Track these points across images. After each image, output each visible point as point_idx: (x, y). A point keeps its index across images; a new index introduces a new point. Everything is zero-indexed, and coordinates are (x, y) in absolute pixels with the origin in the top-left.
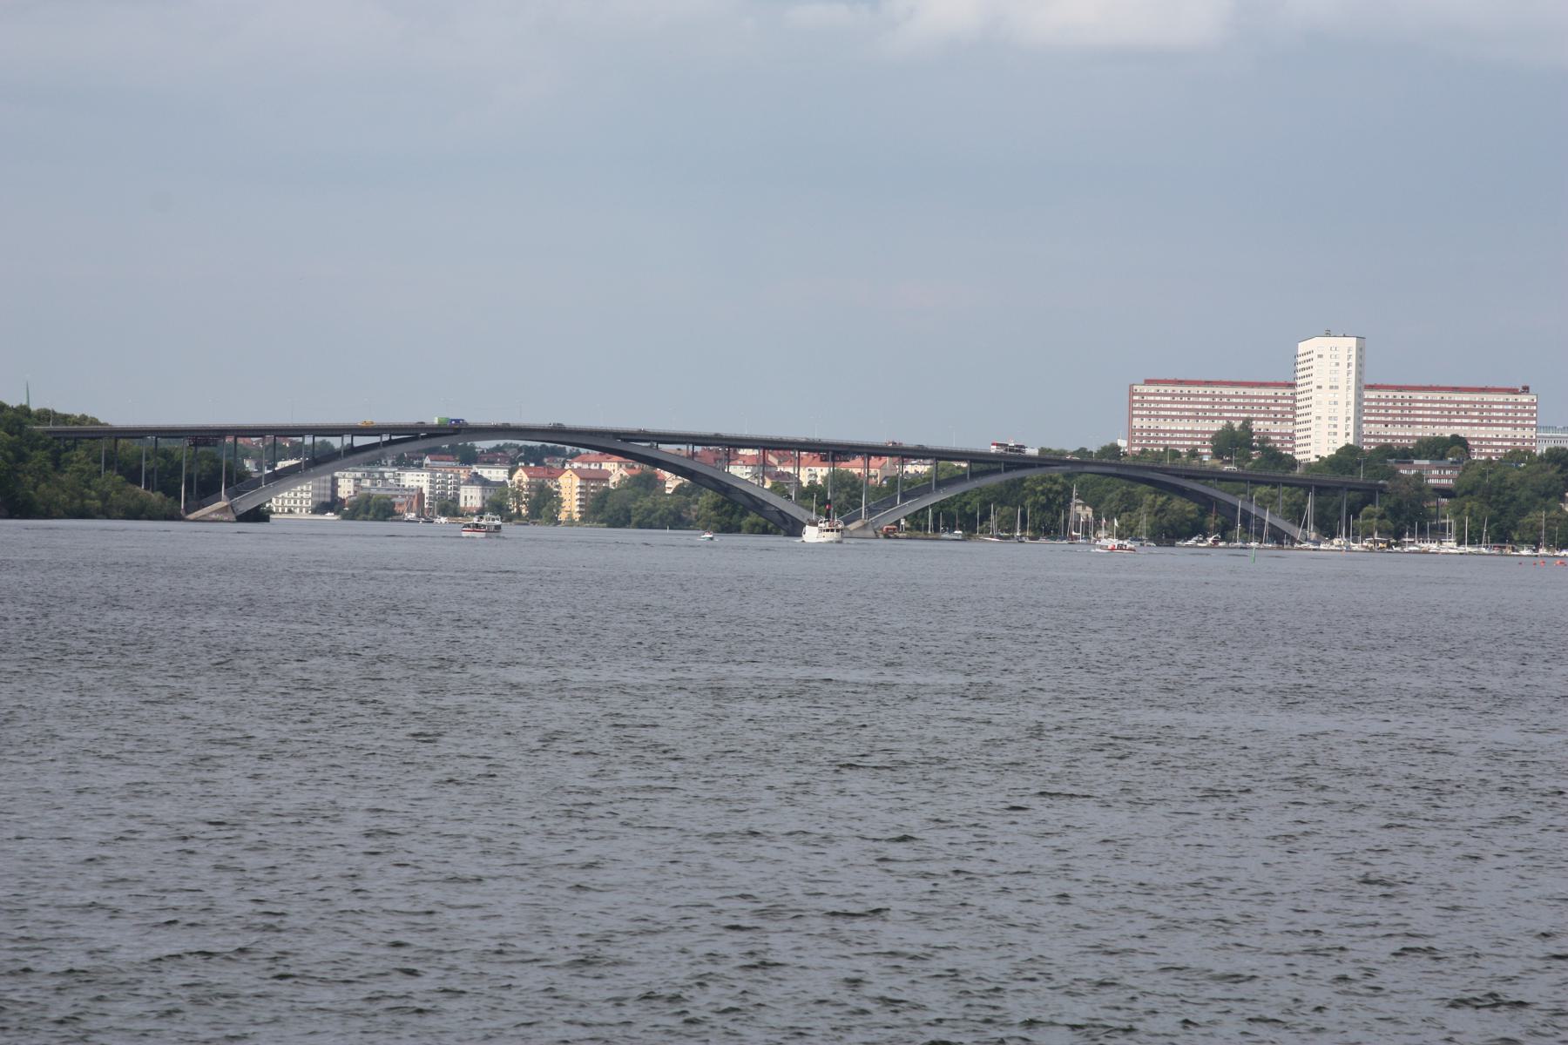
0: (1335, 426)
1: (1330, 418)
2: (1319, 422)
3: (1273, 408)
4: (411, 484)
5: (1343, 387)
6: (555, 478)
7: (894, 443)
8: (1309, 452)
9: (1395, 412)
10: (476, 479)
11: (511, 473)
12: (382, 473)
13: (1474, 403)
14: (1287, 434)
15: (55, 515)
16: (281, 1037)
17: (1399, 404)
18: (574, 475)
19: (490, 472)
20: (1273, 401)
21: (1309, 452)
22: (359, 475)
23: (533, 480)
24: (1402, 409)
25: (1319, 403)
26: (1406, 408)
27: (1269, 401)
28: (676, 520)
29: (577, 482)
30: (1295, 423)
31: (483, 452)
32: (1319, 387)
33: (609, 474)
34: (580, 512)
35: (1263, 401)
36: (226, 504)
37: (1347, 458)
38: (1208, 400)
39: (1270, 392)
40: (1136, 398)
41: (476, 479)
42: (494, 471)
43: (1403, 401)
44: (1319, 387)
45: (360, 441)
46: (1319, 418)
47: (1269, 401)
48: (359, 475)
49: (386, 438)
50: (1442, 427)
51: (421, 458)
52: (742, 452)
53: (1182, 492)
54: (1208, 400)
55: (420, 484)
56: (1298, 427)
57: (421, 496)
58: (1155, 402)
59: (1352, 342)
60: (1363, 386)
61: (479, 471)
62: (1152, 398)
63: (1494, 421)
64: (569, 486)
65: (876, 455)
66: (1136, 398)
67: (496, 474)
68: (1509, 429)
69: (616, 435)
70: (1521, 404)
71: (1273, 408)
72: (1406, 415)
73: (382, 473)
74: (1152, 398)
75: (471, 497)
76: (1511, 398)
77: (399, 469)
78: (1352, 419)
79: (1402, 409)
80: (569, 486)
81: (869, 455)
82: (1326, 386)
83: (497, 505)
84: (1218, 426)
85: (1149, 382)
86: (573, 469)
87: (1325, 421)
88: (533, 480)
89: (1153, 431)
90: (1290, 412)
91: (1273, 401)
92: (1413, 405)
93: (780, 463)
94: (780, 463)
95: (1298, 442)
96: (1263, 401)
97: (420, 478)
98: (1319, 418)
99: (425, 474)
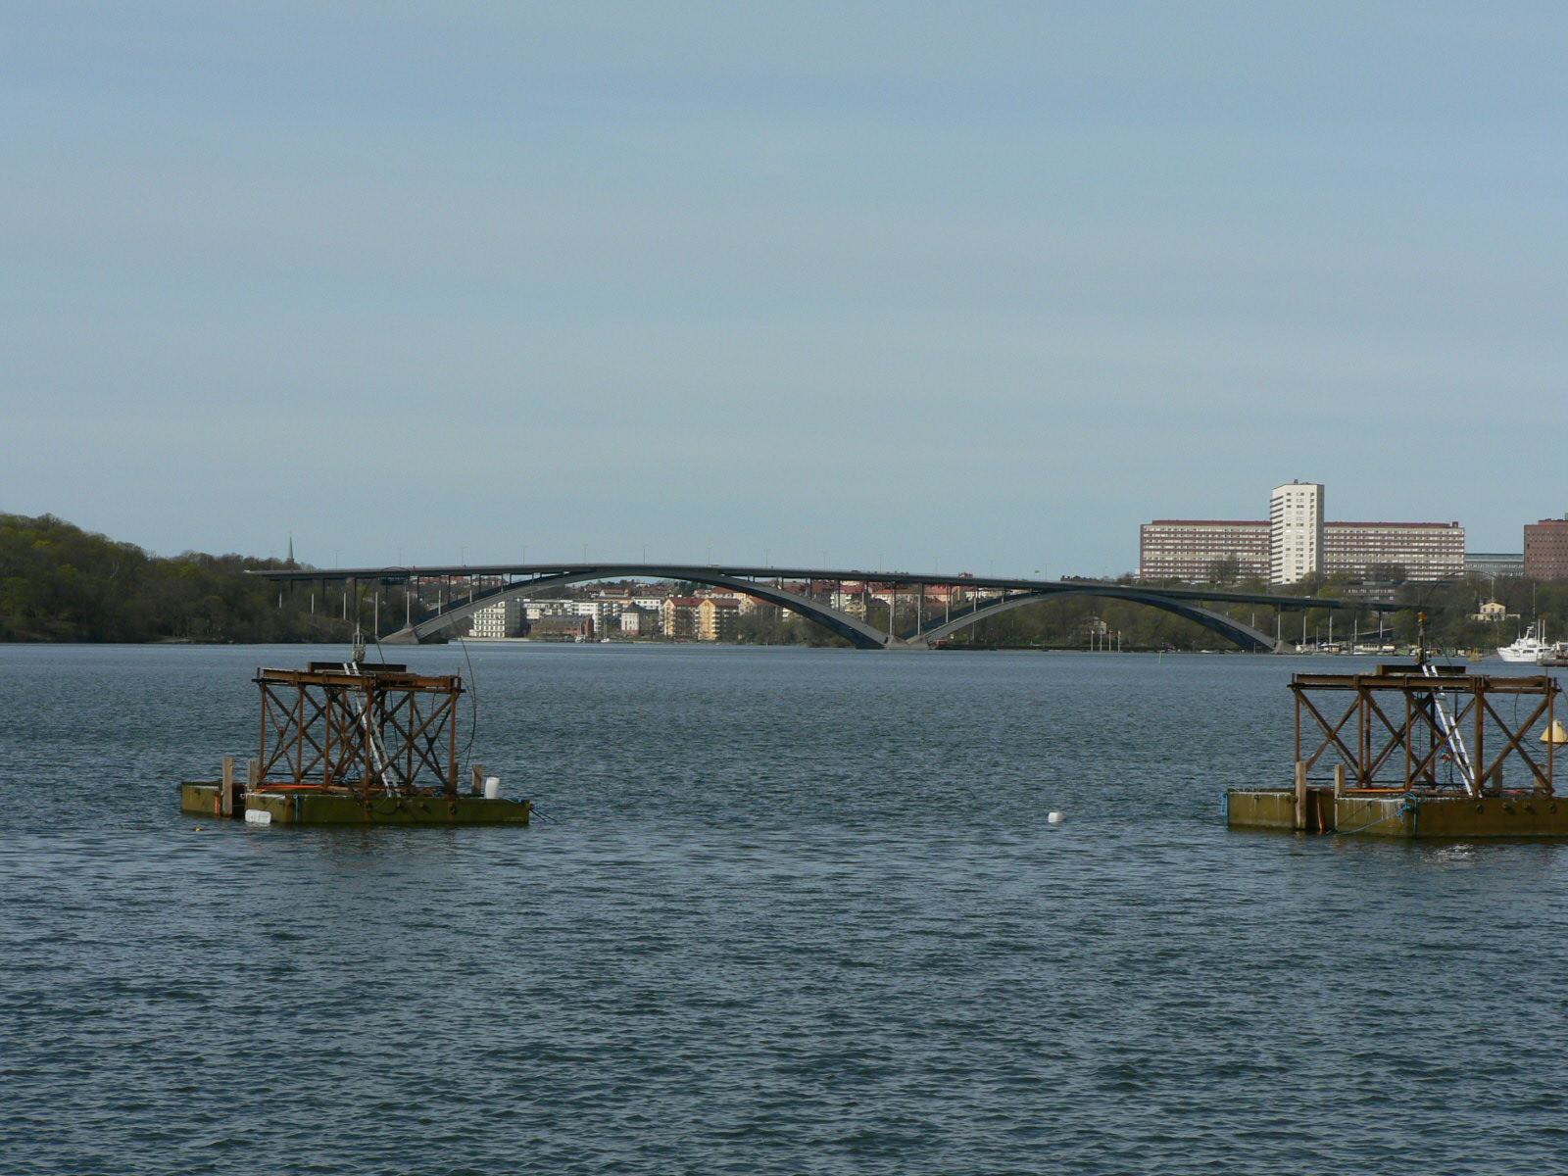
0: (1302, 556)
1: (1297, 549)
2: (1288, 552)
3: (1255, 542)
4: (583, 612)
5: (1307, 524)
6: (696, 607)
7: (966, 575)
8: (1280, 577)
9: (1221, 542)
10: (634, 608)
11: (663, 602)
12: (562, 604)
13: (1257, 534)
14: (1266, 563)
15: (326, 641)
16: (64, 1132)
17: (1355, 538)
18: (711, 604)
19: (645, 602)
20: (1255, 537)
21: (1280, 577)
22: (543, 606)
23: (679, 608)
24: (1358, 541)
25: (1288, 537)
26: (1361, 541)
27: (1251, 537)
28: (790, 638)
29: (713, 609)
30: (1271, 554)
31: (646, 586)
32: (1289, 525)
33: (739, 602)
34: (716, 633)
35: (1246, 536)
36: (410, 630)
37: (1313, 582)
38: (1436, 539)
39: (1252, 529)
40: (1146, 535)
41: (634, 608)
42: (649, 601)
43: (1358, 535)
44: (1289, 525)
45: (516, 578)
46: (1288, 549)
47: (1251, 537)
48: (543, 606)
49: (537, 576)
50: (1390, 556)
51: (598, 592)
52: (845, 583)
53: (1174, 609)
54: (1436, 539)
55: (590, 613)
56: (1274, 557)
57: (591, 622)
58: (1161, 538)
59: (1314, 489)
60: (1322, 524)
61: (637, 601)
62: (1158, 535)
63: (1217, 548)
64: (707, 615)
65: (929, 584)
66: (1146, 535)
67: (650, 603)
68: (1158, 553)
69: (720, 571)
70: (1452, 536)
71: (1255, 542)
72: (1361, 547)
73: (562, 604)
74: (1158, 535)
75: (630, 622)
76: (1444, 532)
77: (574, 601)
78: (1315, 550)
79: (1358, 541)
80: (707, 615)
81: (924, 583)
82: (1294, 524)
83: (650, 628)
84: (1211, 556)
85: (1156, 523)
86: (710, 599)
87: (1293, 552)
88: (679, 608)
89: (1160, 561)
90: (1268, 546)
91: (1255, 537)
92: (1366, 538)
93: (874, 591)
94: (874, 591)
95: (1274, 569)
96: (1246, 536)
97: (591, 608)
98: (1288, 549)
99: (595, 604)
